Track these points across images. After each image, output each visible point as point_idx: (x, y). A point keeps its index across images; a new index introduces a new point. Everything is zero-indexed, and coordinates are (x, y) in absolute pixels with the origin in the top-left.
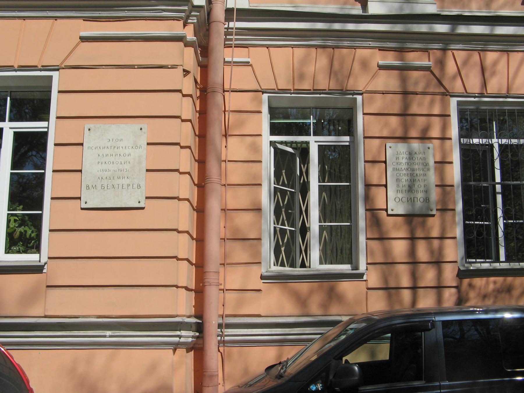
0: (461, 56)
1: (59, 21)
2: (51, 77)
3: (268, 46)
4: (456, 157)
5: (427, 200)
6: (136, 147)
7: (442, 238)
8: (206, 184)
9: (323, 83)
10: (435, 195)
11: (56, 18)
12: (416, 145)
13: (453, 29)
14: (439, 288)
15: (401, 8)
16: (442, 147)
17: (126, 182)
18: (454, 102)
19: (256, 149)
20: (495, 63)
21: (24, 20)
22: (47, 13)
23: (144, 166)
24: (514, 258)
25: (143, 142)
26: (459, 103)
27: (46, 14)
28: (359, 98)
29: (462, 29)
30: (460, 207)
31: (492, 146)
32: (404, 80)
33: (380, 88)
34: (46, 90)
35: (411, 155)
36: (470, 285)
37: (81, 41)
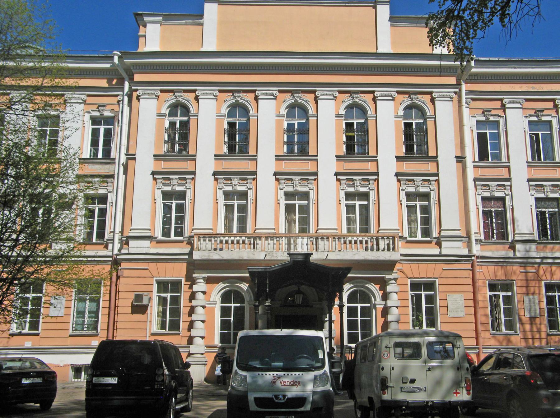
0: (544, 268)
3: (487, 266)
4: (544, 299)
5: (535, 313)
6: (461, 300)
7: (540, 324)
9: (503, 278)
10: (538, 312)
12: (531, 297)
13: (542, 261)
14: (540, 339)
15: (525, 255)
16: (539, 296)
17: (459, 310)
18: (543, 283)
19: (485, 297)
20: (555, 271)
23: (464, 305)
25: (463, 299)
26: (545, 283)
28: (514, 282)
29: (545, 261)
30: (546, 315)
31: (555, 295)
32: (526, 276)
33: (519, 279)
35: (530, 300)
36: (551, 339)
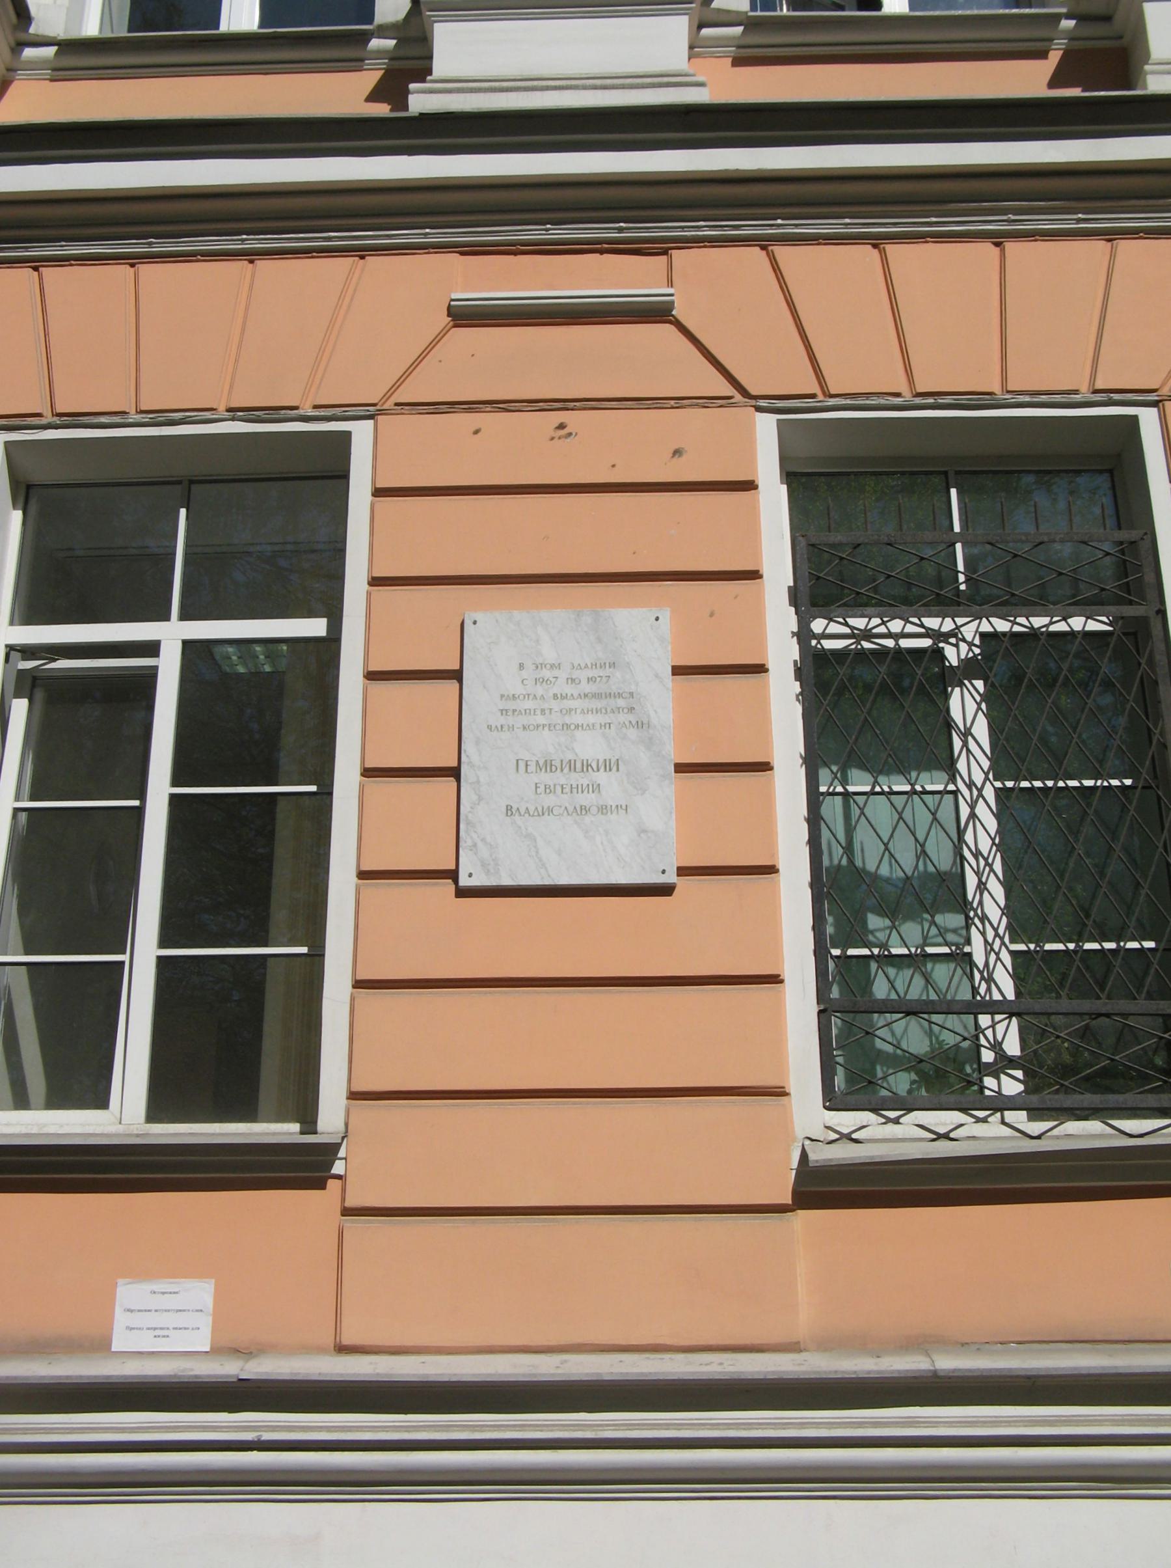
1: (373, 261)
2: (347, 435)
8: (904, 775)
11: (362, 252)
21: (251, 262)
22: (547, 230)
24: (971, 1067)
27: (544, 232)
34: (985, 469)
37: (452, 323)
